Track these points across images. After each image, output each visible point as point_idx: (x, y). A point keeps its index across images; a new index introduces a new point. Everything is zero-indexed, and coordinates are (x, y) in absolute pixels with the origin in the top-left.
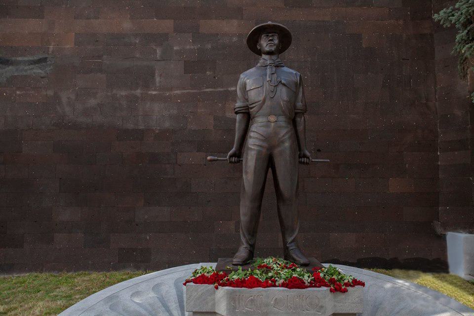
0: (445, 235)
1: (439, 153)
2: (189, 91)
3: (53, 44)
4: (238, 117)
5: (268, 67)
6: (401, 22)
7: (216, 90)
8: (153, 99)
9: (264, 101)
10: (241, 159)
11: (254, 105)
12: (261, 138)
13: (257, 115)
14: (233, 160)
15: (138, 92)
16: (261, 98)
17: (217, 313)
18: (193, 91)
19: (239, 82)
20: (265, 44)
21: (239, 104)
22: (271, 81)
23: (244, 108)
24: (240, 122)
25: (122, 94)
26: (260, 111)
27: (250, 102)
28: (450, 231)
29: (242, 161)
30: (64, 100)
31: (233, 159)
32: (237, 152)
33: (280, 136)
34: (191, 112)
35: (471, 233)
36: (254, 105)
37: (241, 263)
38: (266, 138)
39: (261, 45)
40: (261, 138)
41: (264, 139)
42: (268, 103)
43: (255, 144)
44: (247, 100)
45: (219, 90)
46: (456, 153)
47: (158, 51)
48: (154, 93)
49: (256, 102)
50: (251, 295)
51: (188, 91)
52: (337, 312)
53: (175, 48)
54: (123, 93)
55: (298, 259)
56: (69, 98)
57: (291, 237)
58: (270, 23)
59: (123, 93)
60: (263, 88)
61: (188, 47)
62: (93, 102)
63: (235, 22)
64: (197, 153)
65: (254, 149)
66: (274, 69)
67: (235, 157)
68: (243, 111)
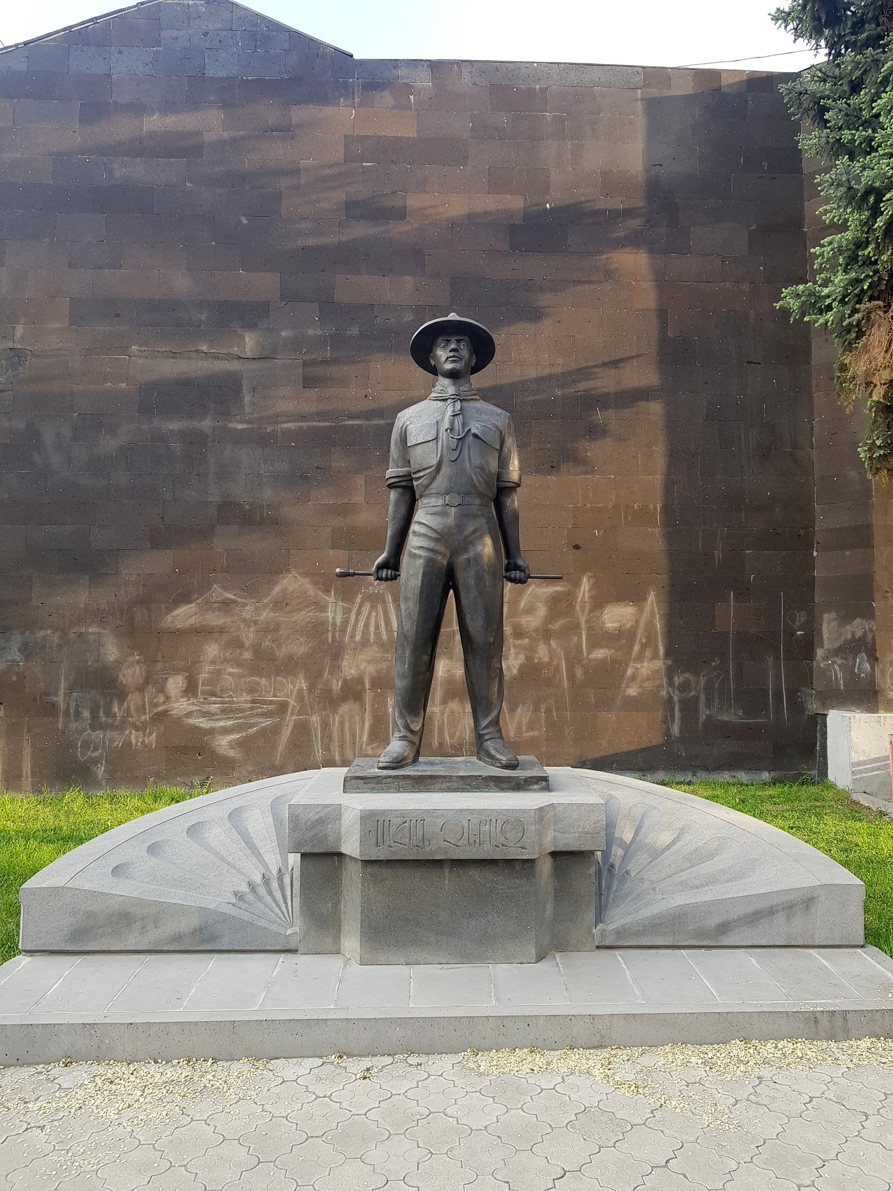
0: (825, 716)
1: (815, 554)
2: (315, 424)
3: (23, 320)
4: (393, 495)
5: (449, 401)
6: (746, 287)
7: (371, 422)
8: (239, 438)
9: (439, 466)
10: (398, 573)
11: (421, 474)
12: (434, 535)
13: (426, 493)
14: (384, 576)
15: (206, 424)
16: (435, 462)
17: (345, 854)
18: (322, 424)
19: (395, 430)
20: (442, 355)
21: (393, 471)
22: (451, 430)
23: (404, 479)
24: (397, 505)
25: (171, 427)
26: (433, 485)
27: (413, 467)
28: (832, 708)
29: (399, 575)
30: (49, 438)
31: (384, 573)
32: (392, 561)
33: (466, 532)
34: (318, 468)
35: (891, 711)
36: (421, 474)
37: (392, 765)
38: (441, 536)
39: (435, 358)
40: (434, 535)
41: (438, 536)
42: (446, 470)
43: (422, 547)
44: (408, 463)
45: (375, 422)
46: (848, 553)
47: (247, 340)
48: (240, 426)
49: (425, 469)
50: (405, 820)
51: (311, 424)
52: (558, 849)
53: (283, 334)
54: (175, 425)
55: (499, 756)
56: (58, 435)
57: (487, 716)
58: (453, 316)
59: (175, 425)
60: (437, 443)
61: (311, 332)
62: (109, 444)
63: (409, 281)
64: (331, 552)
65: (420, 557)
66: (458, 405)
67: (388, 569)
68: (403, 484)
